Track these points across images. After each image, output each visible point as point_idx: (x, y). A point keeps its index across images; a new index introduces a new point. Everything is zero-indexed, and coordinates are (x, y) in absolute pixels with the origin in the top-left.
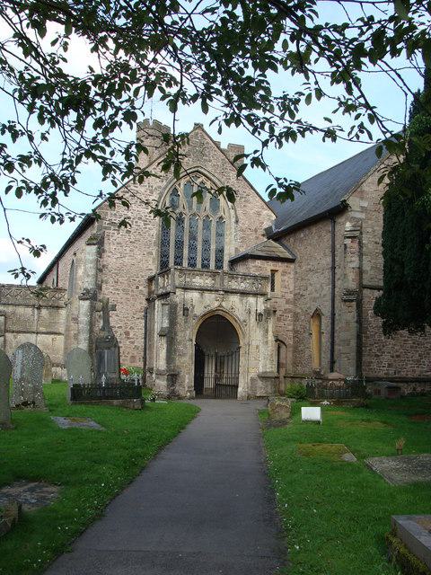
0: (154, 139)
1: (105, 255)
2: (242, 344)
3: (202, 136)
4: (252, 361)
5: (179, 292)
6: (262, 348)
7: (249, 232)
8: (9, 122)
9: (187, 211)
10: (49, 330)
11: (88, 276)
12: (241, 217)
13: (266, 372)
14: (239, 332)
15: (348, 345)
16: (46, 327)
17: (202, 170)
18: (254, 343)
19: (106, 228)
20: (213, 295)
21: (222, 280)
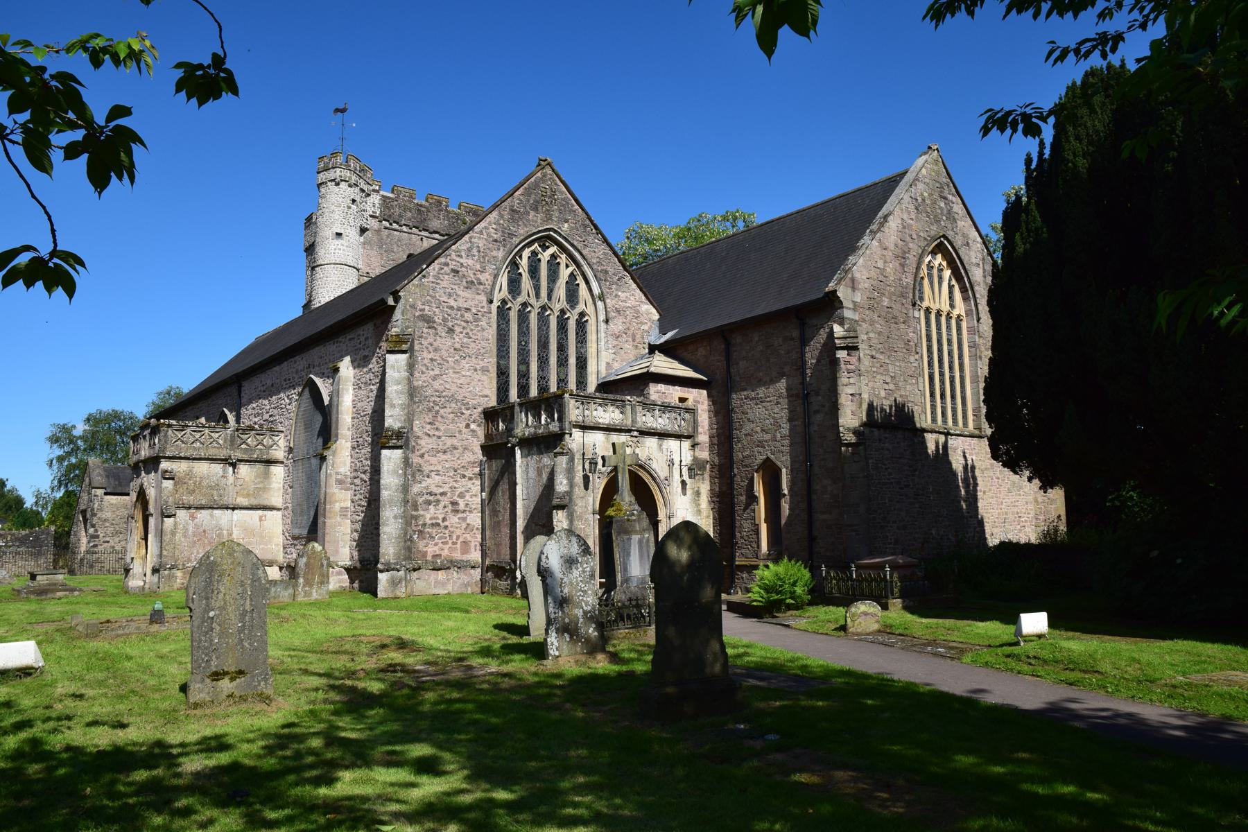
9: (533, 300)
10: (254, 502)
16: (248, 496)
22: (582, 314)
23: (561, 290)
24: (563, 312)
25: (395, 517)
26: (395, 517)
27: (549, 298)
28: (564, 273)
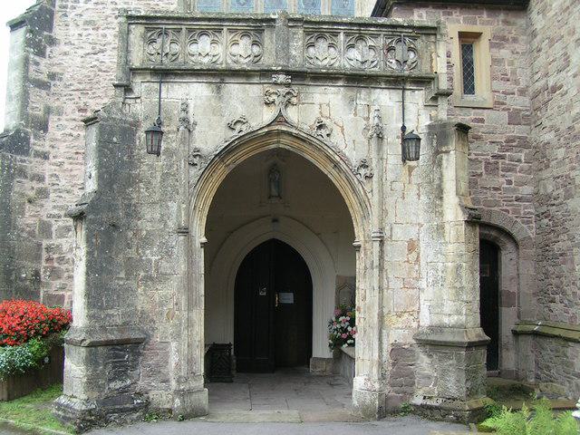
20: (255, 90)
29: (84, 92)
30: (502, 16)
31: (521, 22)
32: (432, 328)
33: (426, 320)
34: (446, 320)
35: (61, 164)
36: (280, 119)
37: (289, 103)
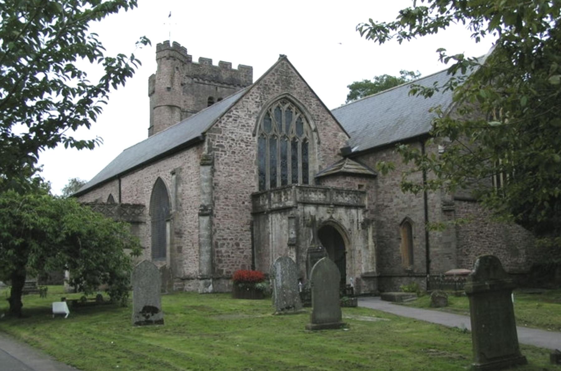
0: (175, 60)
1: (216, 174)
2: (347, 250)
3: (287, 66)
4: (357, 266)
5: (300, 207)
6: (363, 253)
7: (329, 152)
8: (132, 58)
9: (278, 133)
11: (204, 193)
12: (322, 137)
13: (368, 273)
14: (345, 239)
15: (449, 247)
17: (289, 97)
18: (357, 248)
19: (215, 149)
20: (325, 209)
21: (331, 194)
22: (305, 140)
23: (293, 127)
24: (294, 139)
25: (207, 252)
26: (207, 252)
27: (287, 131)
28: (295, 117)
29: (226, 192)
30: (369, 180)
31: (374, 181)
32: (366, 273)
33: (363, 271)
34: (370, 271)
35: (220, 219)
36: (331, 217)
37: (333, 213)
